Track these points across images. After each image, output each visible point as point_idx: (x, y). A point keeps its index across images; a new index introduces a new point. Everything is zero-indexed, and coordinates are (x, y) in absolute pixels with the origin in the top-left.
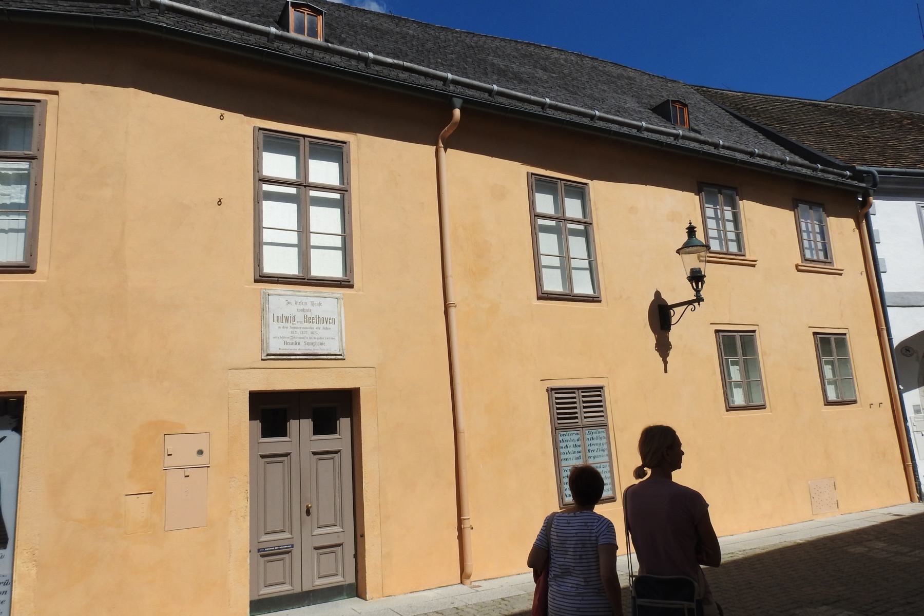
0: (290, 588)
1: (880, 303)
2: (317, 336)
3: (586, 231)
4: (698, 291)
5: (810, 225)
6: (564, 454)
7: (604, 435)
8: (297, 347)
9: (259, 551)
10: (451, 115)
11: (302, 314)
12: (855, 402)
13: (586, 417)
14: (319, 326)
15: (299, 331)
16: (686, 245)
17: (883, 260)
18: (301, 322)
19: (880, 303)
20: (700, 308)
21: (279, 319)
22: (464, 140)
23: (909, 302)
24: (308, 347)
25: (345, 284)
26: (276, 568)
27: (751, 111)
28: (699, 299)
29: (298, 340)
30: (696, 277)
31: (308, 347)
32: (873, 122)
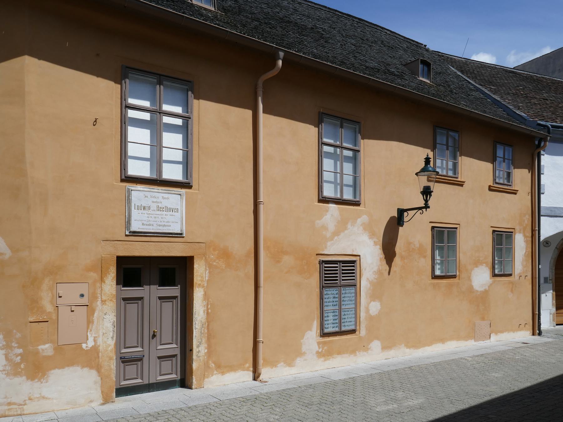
0: (141, 381)
4: (426, 201)
6: (326, 302)
7: (354, 291)
8: (151, 227)
9: (121, 358)
10: (275, 64)
13: (343, 280)
15: (153, 216)
16: (423, 170)
17: (544, 185)
18: (154, 210)
19: (536, 212)
20: (426, 212)
21: (139, 208)
23: (555, 214)
24: (159, 227)
25: (185, 185)
26: (132, 369)
27: (471, 73)
28: (427, 207)
30: (427, 192)
32: (550, 88)
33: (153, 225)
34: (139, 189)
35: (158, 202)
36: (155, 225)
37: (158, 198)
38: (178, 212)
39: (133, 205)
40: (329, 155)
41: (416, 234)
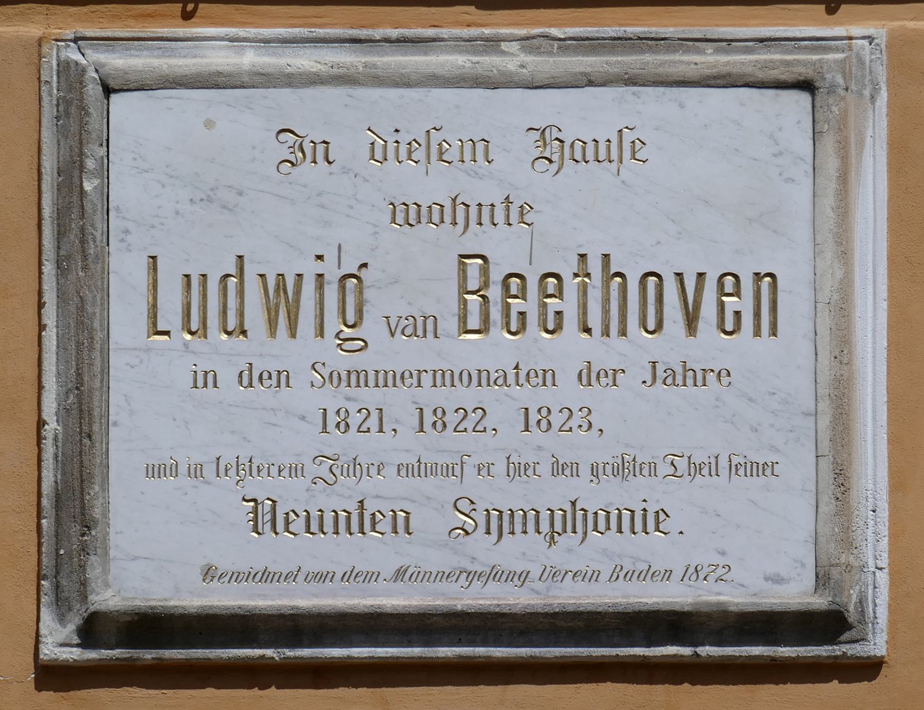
2: (583, 448)
8: (377, 552)
11: (444, 489)
14: (604, 352)
15: (400, 402)
18: (422, 327)
24: (483, 550)
29: (384, 491)
31: (483, 550)
33: (402, 524)
34: (218, 58)
35: (483, 214)
36: (431, 521)
37: (480, 148)
38: (767, 319)
39: (125, 271)
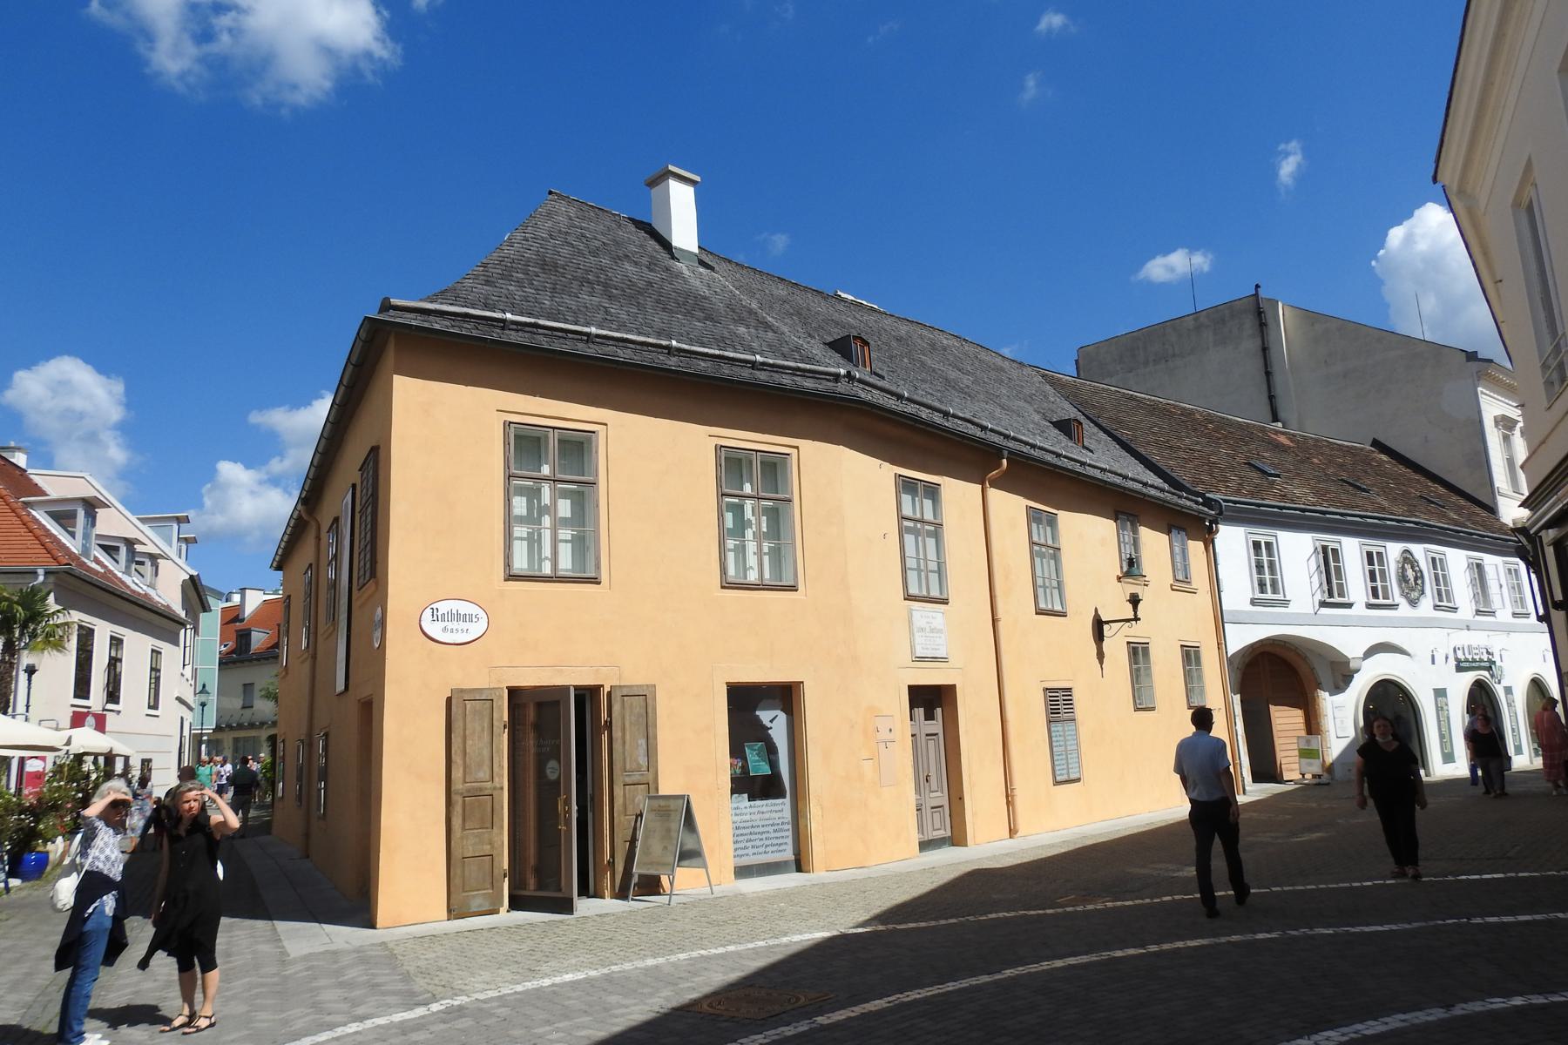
1: (1220, 620)
3: (937, 531)
5: (1128, 536)
10: (1000, 465)
12: (1153, 709)
19: (1220, 620)
21: (940, 631)
22: (1003, 484)
28: (1136, 619)
30: (1135, 601)
40: (909, 530)
41: (1116, 643)
